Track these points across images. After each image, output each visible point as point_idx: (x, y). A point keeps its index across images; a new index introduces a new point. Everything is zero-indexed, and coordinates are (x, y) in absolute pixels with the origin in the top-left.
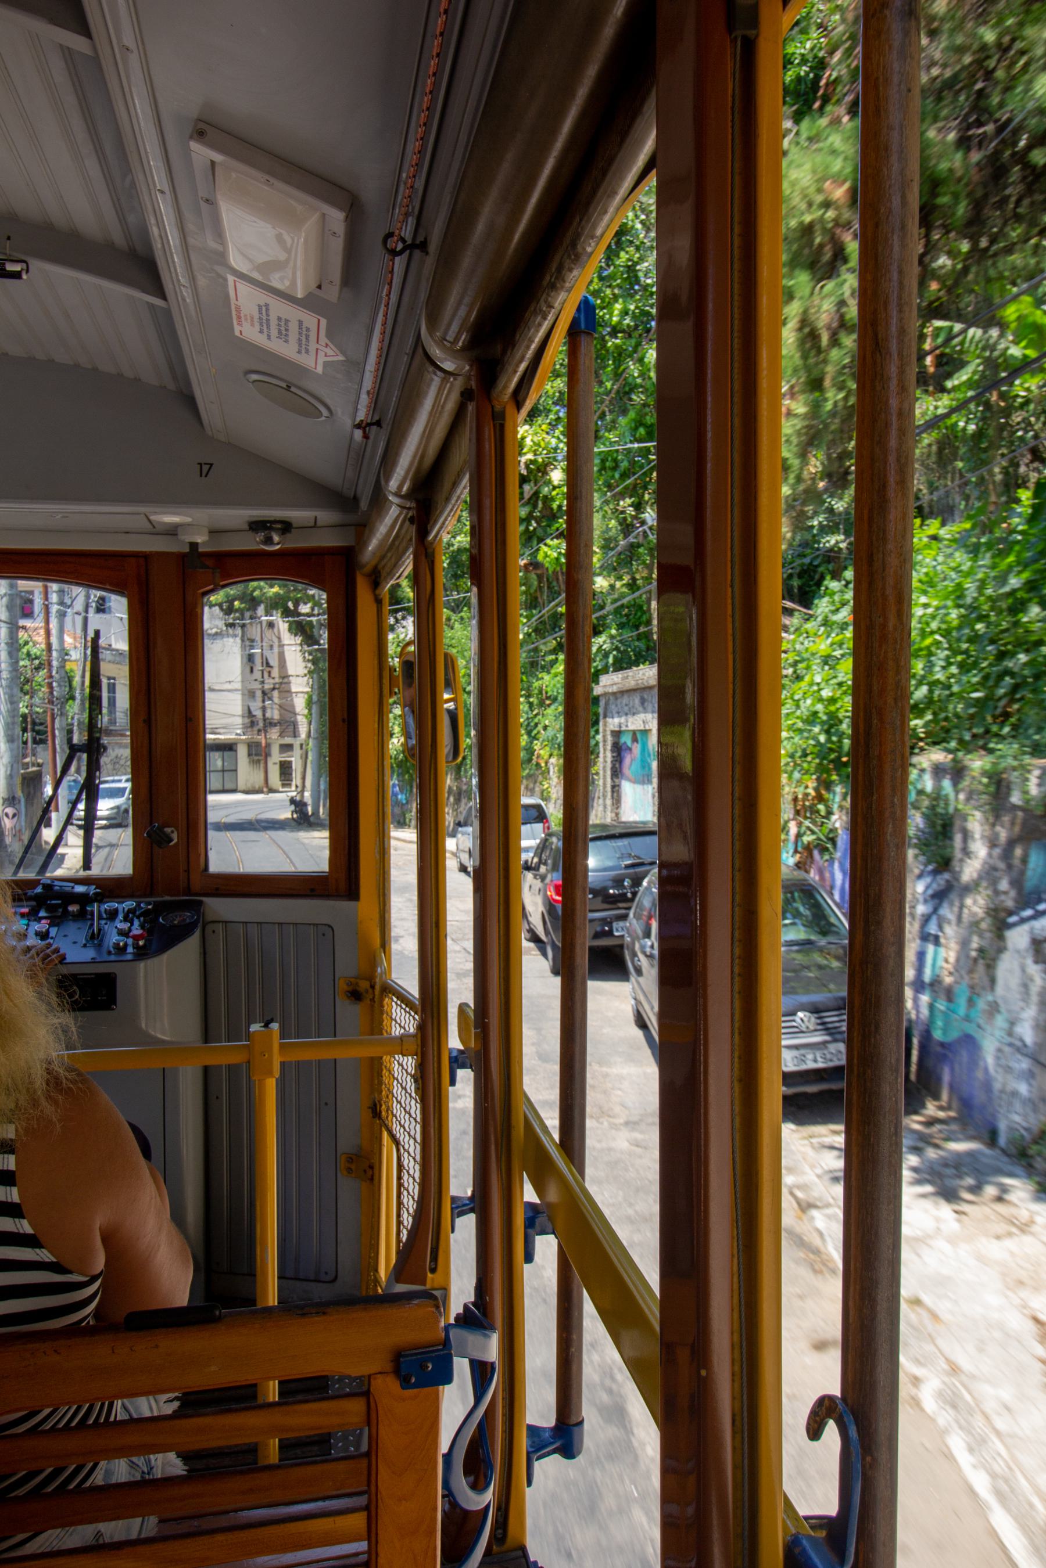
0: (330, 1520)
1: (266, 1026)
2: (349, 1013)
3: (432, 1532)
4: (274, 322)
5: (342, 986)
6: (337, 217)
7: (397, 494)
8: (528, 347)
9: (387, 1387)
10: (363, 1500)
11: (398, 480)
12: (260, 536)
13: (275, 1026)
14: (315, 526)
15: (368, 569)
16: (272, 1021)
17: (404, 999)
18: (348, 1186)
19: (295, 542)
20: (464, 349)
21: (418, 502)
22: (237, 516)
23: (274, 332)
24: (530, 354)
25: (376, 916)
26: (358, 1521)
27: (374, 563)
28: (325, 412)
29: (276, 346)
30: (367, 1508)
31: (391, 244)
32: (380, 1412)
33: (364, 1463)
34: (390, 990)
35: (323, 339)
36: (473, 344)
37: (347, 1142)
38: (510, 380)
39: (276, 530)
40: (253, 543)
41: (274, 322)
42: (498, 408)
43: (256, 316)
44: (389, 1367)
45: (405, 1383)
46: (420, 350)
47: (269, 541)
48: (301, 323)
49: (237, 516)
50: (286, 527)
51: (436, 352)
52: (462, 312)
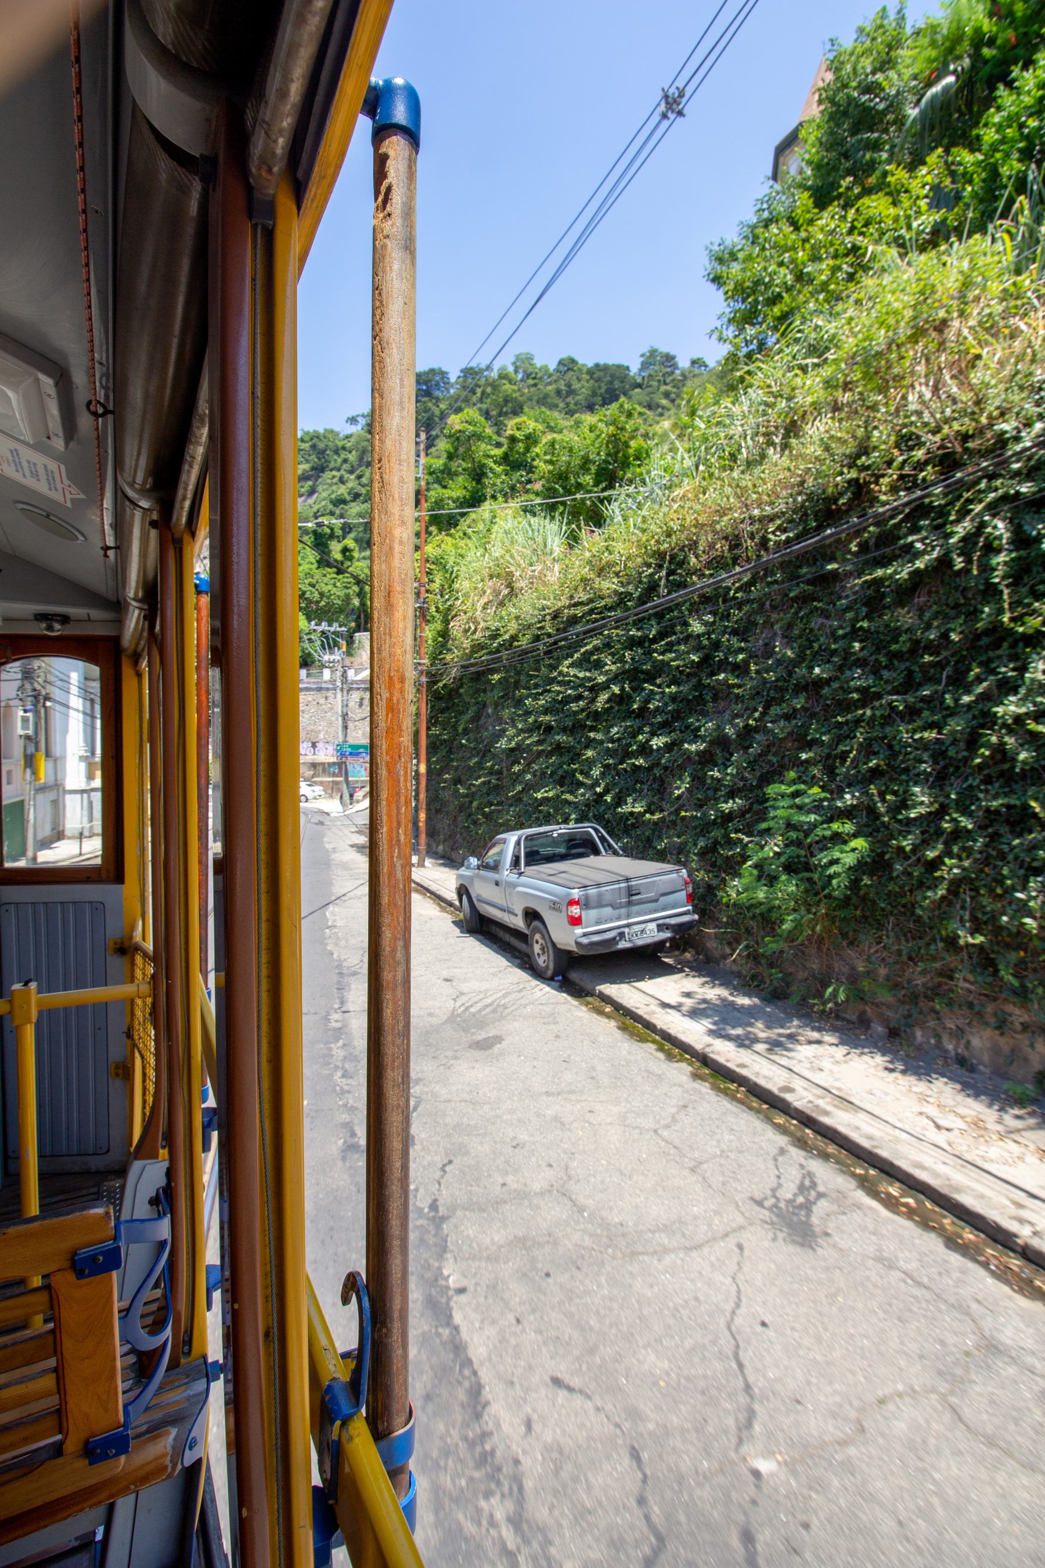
0: (23, 1386)
1: (26, 984)
2: (116, 963)
3: (112, 1376)
4: (25, 465)
5: (111, 944)
6: (47, 382)
7: (135, 599)
8: (186, 489)
9: (65, 1282)
10: (52, 1362)
11: (132, 587)
12: (43, 625)
13: (33, 985)
14: (89, 620)
15: (130, 652)
16: (30, 981)
17: (145, 955)
18: (117, 1085)
19: (70, 630)
20: (151, 490)
21: (149, 604)
22: (32, 608)
23: (28, 473)
24: (190, 495)
25: (137, 894)
26: (49, 1382)
27: (132, 647)
28: (81, 538)
29: (30, 482)
30: (55, 1370)
31: (92, 408)
32: (61, 1298)
33: (51, 1338)
34: (137, 948)
35: (66, 482)
36: (155, 488)
37: (115, 1053)
38: (180, 515)
39: (57, 621)
40: (39, 629)
41: (25, 465)
42: (177, 536)
43: (10, 458)
44: (67, 1264)
45: (80, 1274)
46: (119, 493)
47: (50, 628)
48: (45, 467)
49: (32, 608)
50: (65, 619)
51: (131, 493)
52: (143, 462)
